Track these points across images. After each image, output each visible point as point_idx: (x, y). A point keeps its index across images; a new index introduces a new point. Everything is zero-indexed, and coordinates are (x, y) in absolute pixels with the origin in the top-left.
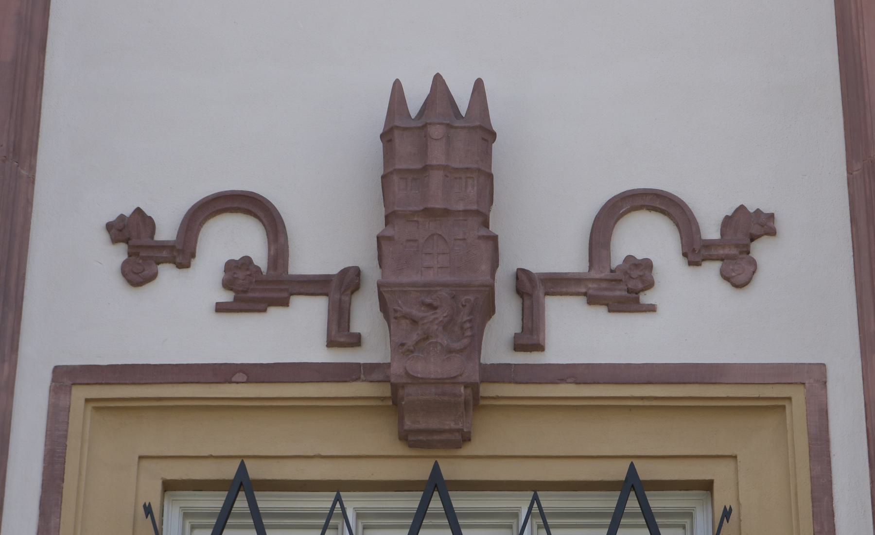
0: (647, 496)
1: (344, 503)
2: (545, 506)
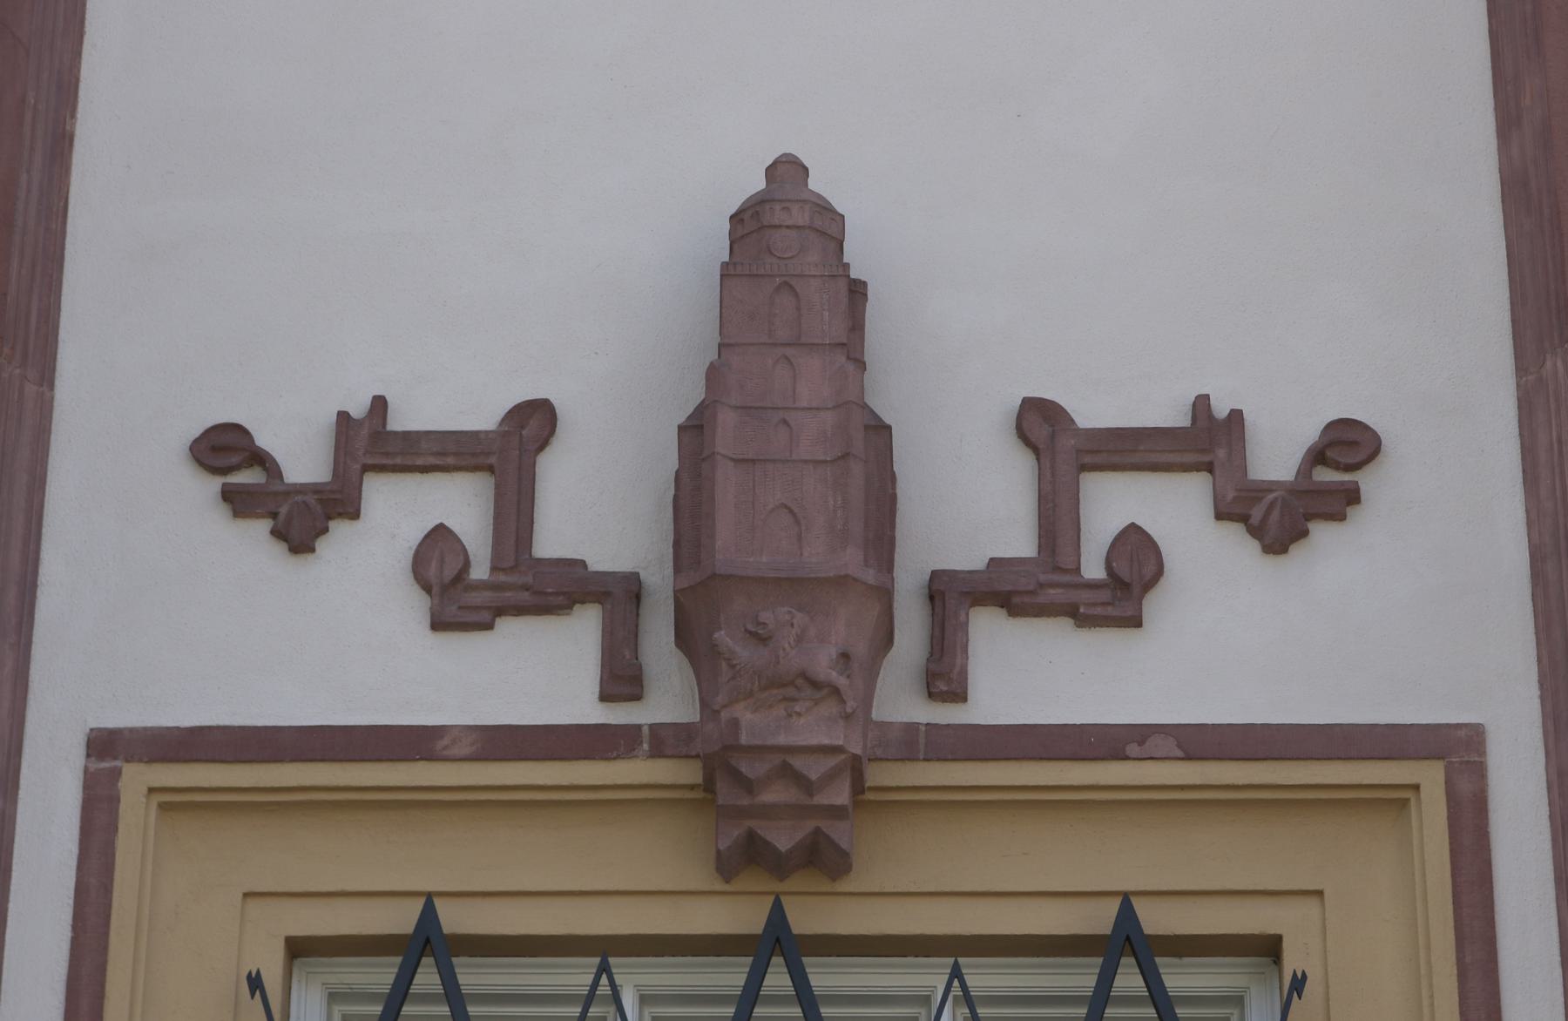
0: (805, 965)
2: (974, 985)
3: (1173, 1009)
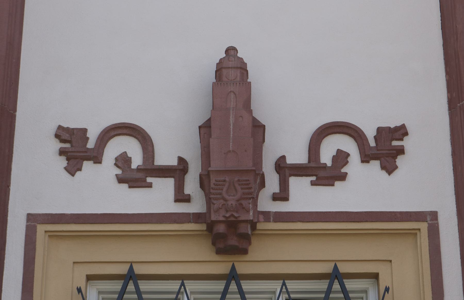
1: (186, 286)
3: (142, 295)
